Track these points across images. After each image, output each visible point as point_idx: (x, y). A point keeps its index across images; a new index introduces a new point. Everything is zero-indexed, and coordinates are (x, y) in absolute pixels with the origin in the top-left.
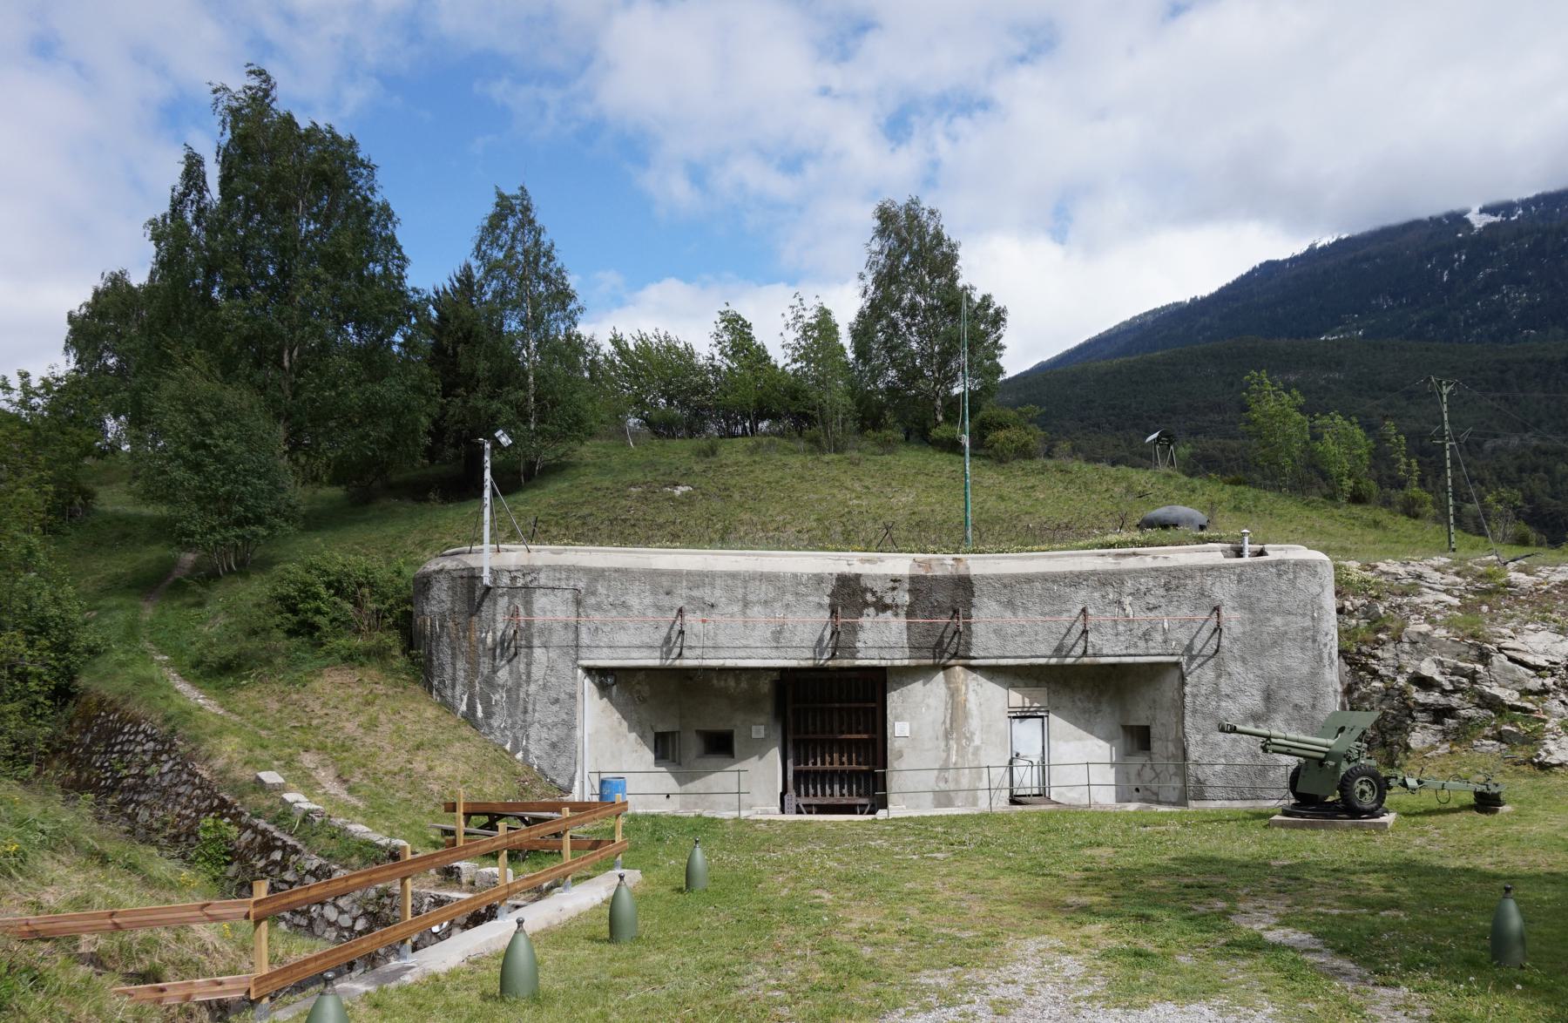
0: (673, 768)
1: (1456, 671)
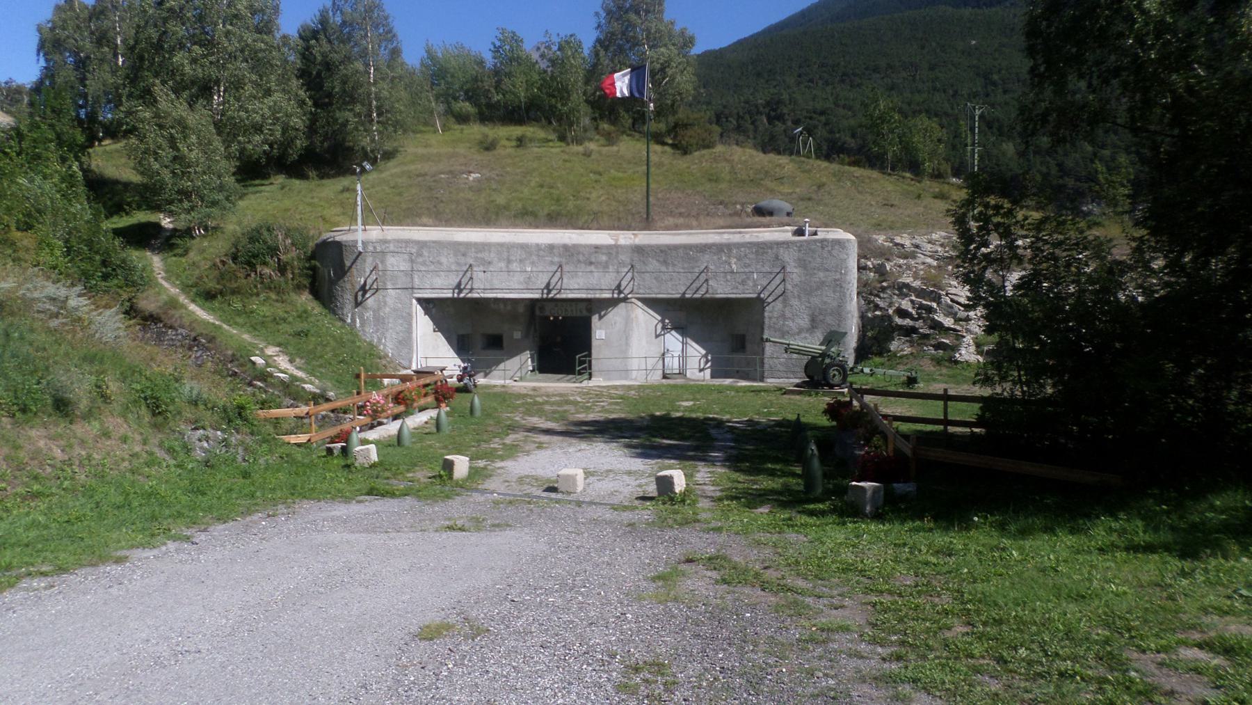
0: (758, 427)
1: (921, 307)
